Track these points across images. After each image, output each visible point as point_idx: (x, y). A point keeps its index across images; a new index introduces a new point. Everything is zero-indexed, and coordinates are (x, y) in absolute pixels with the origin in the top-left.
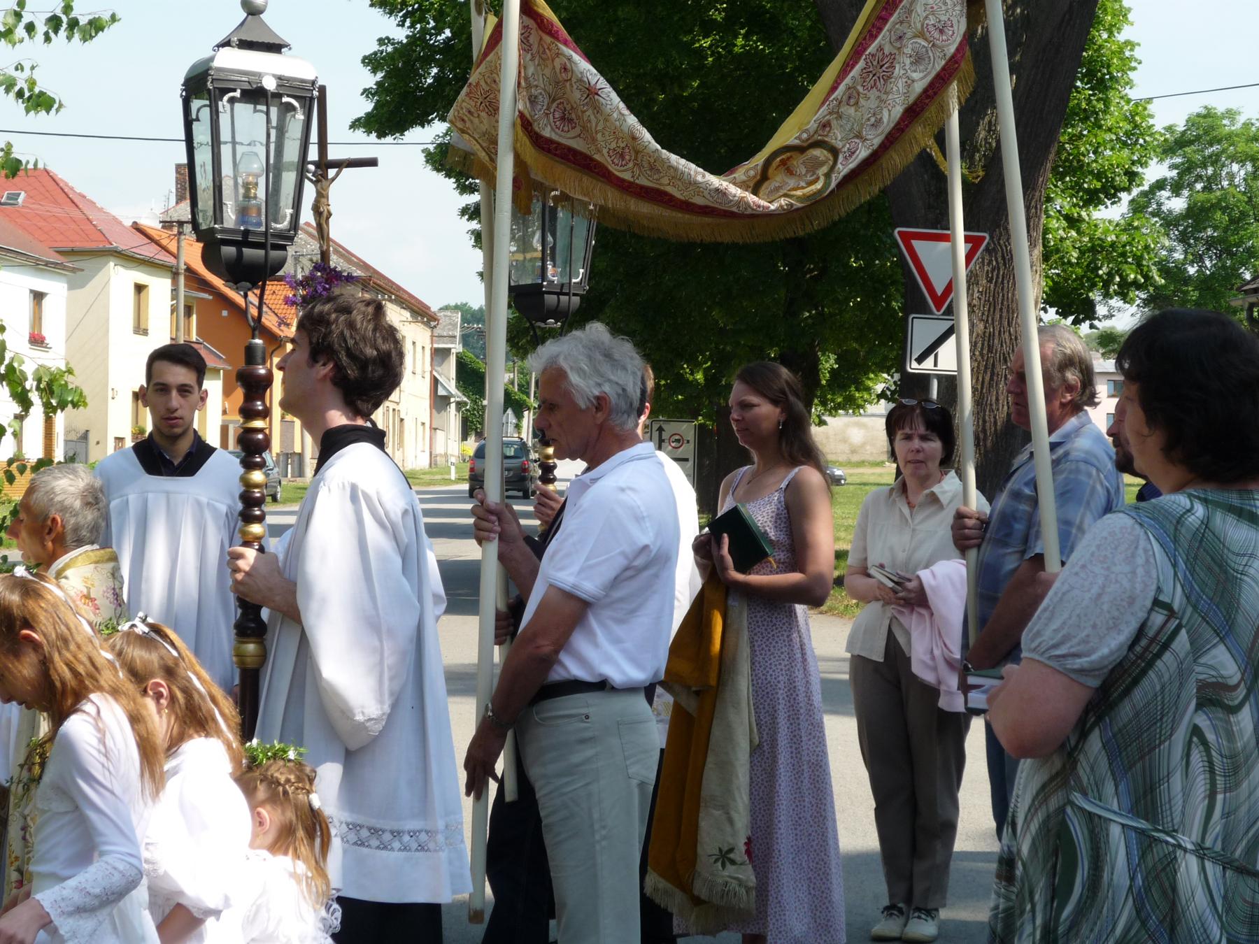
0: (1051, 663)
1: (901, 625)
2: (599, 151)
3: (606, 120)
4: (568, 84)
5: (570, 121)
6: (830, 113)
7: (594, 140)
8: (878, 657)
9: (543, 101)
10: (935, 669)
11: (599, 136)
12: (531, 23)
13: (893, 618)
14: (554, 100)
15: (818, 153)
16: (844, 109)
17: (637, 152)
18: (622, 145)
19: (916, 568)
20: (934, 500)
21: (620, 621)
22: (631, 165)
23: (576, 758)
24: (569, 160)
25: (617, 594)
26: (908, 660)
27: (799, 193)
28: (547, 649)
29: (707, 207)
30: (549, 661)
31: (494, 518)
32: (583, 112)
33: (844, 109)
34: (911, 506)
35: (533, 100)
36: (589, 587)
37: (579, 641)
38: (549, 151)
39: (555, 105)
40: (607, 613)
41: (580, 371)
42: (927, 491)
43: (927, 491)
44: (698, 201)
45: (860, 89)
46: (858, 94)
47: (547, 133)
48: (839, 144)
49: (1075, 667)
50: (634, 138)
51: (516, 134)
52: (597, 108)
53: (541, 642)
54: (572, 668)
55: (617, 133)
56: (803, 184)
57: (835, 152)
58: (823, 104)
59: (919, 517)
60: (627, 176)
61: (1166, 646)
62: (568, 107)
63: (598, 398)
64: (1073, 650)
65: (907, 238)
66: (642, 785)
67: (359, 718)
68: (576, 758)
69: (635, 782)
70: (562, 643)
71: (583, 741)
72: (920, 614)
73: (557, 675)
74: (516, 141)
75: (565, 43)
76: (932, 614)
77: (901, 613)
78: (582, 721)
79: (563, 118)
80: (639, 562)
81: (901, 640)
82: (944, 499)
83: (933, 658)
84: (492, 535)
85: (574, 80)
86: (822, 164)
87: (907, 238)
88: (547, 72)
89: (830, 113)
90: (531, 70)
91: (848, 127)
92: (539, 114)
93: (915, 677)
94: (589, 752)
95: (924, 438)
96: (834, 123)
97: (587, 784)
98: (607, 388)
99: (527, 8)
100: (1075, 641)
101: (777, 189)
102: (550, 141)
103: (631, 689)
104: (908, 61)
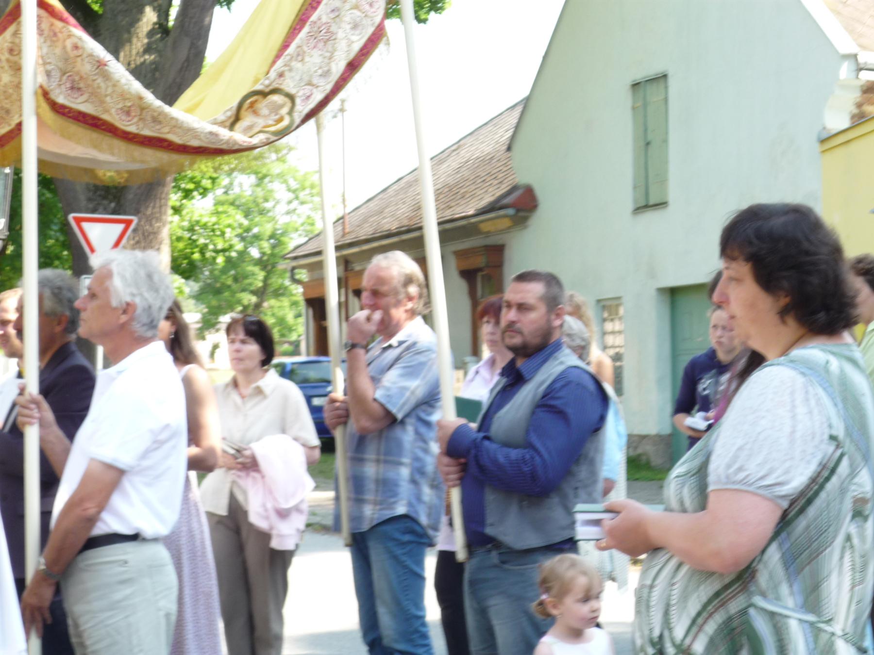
0: (761, 492)
1: (239, 487)
2: (107, 111)
3: (114, 86)
4: (79, 59)
5: (79, 89)
6: (285, 65)
7: (102, 102)
8: (223, 511)
9: (56, 74)
10: (267, 518)
11: (108, 99)
12: (43, 13)
13: (234, 482)
14: (64, 74)
15: (276, 98)
16: (293, 64)
17: (142, 109)
18: (129, 104)
19: (250, 442)
20: (259, 391)
21: (148, 485)
22: (135, 120)
23: (118, 596)
24: (79, 121)
25: (146, 463)
26: (245, 513)
27: (273, 129)
28: (92, 511)
29: (200, 148)
30: (92, 521)
31: (33, 406)
32: (94, 80)
33: (293, 64)
34: (243, 397)
35: (48, 74)
36: (123, 458)
37: (117, 500)
38: (63, 114)
39: (65, 78)
40: (137, 480)
41: (123, 277)
42: (254, 385)
43: (254, 385)
44: (195, 143)
45: (305, 49)
46: (304, 52)
47: (61, 100)
48: (293, 91)
49: (783, 493)
50: (141, 98)
51: (37, 101)
52: (106, 76)
53: (88, 505)
54: (109, 524)
55: (124, 95)
56: (271, 122)
57: (291, 98)
58: (278, 56)
59: (250, 404)
60: (132, 129)
61: (833, 471)
62: (77, 78)
63: (128, 304)
64: (780, 480)
65: (78, 221)
66: (168, 615)
67: (43, 567)
68: (118, 596)
69: (162, 613)
70: (102, 506)
71: (123, 582)
72: (254, 478)
73: (100, 529)
74: (38, 107)
75: (75, 26)
76: (263, 477)
77: (239, 476)
78: (121, 566)
79: (72, 88)
80: (162, 437)
81: (240, 497)
82: (267, 390)
83: (266, 510)
84: (35, 421)
85: (85, 55)
86: (282, 106)
87: (78, 221)
88: (58, 51)
89: (285, 65)
90: (45, 50)
91: (298, 78)
92: (54, 85)
93: (251, 525)
94: (127, 591)
95: (243, 342)
96: (287, 74)
97: (127, 617)
98: (137, 300)
99: (42, 4)
100: (779, 472)
101: (250, 127)
102: (63, 107)
103: (155, 540)
104: (348, 27)
